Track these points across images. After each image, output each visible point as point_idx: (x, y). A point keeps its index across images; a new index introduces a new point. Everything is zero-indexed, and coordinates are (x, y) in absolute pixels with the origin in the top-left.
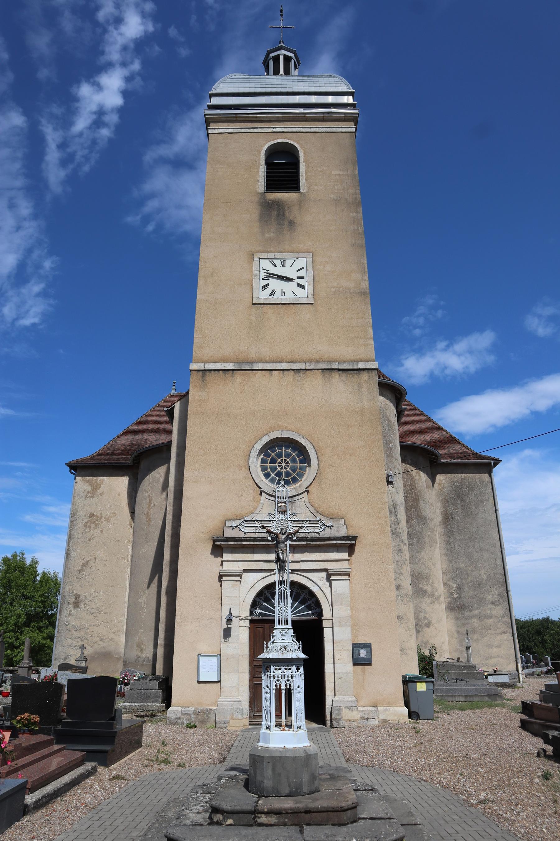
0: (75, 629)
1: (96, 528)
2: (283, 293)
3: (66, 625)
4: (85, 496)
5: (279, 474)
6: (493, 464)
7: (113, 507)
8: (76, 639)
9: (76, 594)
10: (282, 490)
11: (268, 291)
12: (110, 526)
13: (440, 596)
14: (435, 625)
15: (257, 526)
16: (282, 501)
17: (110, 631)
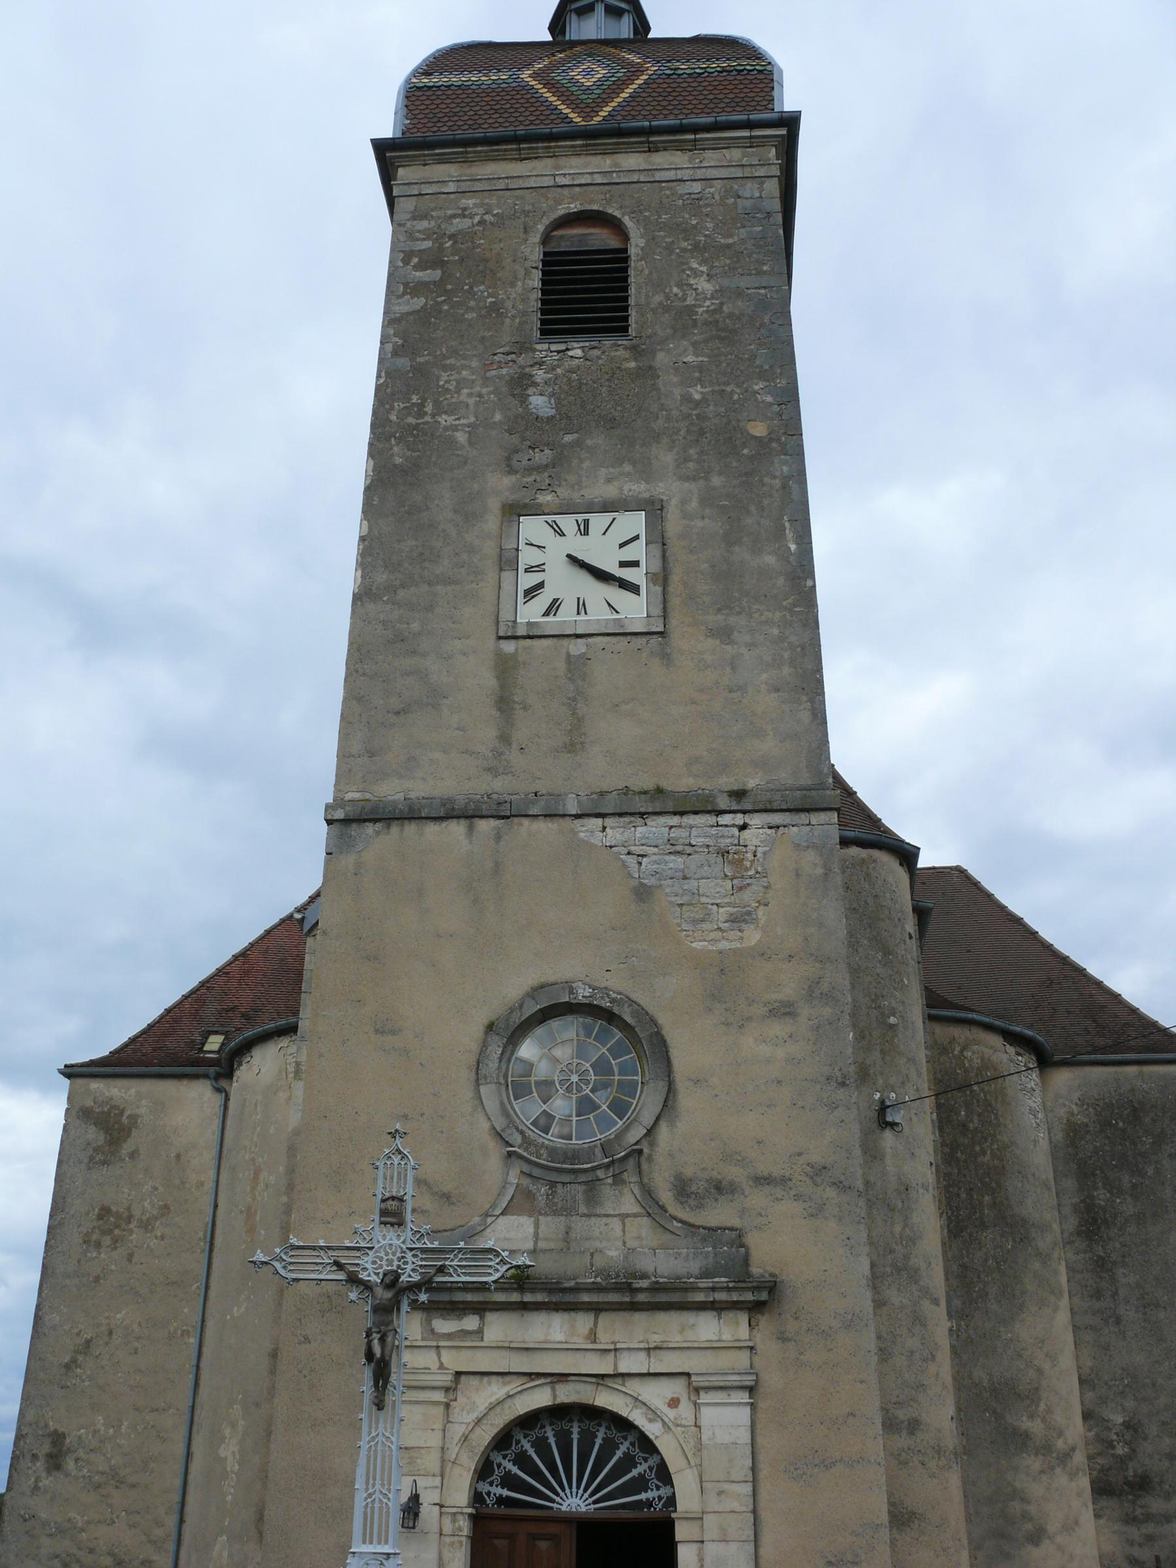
0: (48, 1532)
1: (116, 1248)
2: (581, 607)
3: (25, 1520)
4: (86, 1160)
7: (161, 1189)
9: (56, 1431)
10: (396, 1163)
12: (153, 1243)
13: (1073, 1449)
14: (1059, 1539)
15: (323, 1263)
16: (394, 1194)
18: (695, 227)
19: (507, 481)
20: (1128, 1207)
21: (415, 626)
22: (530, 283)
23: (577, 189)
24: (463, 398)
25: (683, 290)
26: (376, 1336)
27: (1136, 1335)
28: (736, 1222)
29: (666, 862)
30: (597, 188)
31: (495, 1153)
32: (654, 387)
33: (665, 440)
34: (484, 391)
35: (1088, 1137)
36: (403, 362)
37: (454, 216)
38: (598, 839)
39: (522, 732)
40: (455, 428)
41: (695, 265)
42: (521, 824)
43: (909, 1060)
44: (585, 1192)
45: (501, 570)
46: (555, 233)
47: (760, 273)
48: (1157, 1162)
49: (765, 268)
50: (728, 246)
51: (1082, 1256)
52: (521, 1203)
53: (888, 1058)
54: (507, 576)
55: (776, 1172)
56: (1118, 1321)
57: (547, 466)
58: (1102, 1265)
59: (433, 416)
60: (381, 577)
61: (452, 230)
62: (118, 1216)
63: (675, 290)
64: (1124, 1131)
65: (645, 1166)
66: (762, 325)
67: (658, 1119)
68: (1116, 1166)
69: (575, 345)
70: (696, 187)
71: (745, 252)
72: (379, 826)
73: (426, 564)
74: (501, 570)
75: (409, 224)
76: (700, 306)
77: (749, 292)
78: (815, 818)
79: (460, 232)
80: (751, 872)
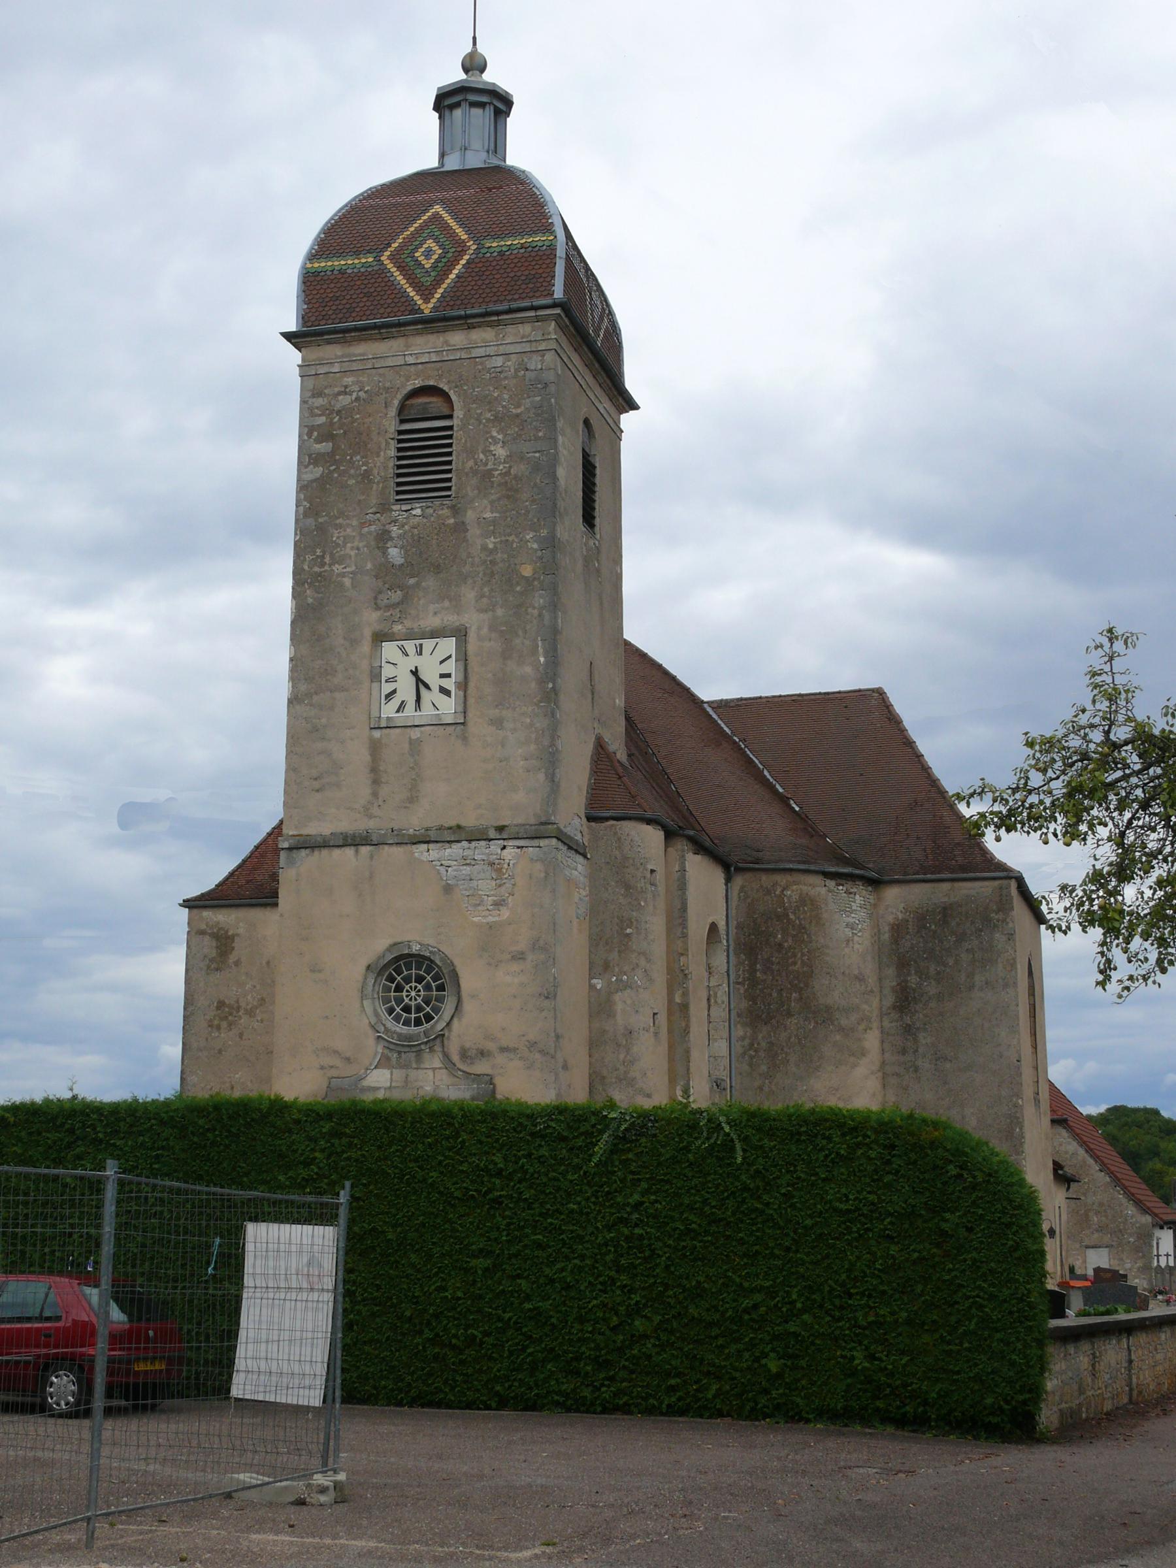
1: (231, 1029)
4: (205, 968)
5: (407, 1009)
7: (258, 987)
11: (395, 703)
12: (256, 1025)
18: (496, 399)
19: (375, 615)
20: (932, 989)
21: (324, 721)
22: (388, 452)
23: (420, 366)
24: (348, 551)
25: (485, 455)
27: (928, 1080)
28: (489, 1072)
29: (461, 871)
30: (433, 365)
31: (372, 1035)
32: (465, 540)
33: (470, 581)
34: (361, 545)
35: (908, 937)
36: (310, 522)
37: (339, 393)
38: (425, 857)
39: (384, 791)
40: (343, 575)
41: (495, 434)
42: (383, 849)
44: (416, 1056)
45: (372, 681)
46: (407, 402)
47: (537, 439)
49: (540, 434)
50: (517, 416)
51: (894, 1024)
52: (385, 1062)
54: (375, 685)
55: (511, 1045)
56: (916, 1069)
57: (398, 603)
58: (908, 1030)
59: (330, 565)
60: (303, 687)
61: (338, 407)
63: (482, 456)
64: (935, 932)
65: (446, 1042)
66: (535, 484)
67: (452, 1017)
68: (926, 958)
69: (418, 505)
70: (499, 362)
71: (529, 420)
72: (308, 851)
73: (329, 677)
74: (372, 681)
75: (311, 400)
76: (497, 470)
77: (529, 455)
78: (543, 843)
79: (344, 408)
80: (506, 876)
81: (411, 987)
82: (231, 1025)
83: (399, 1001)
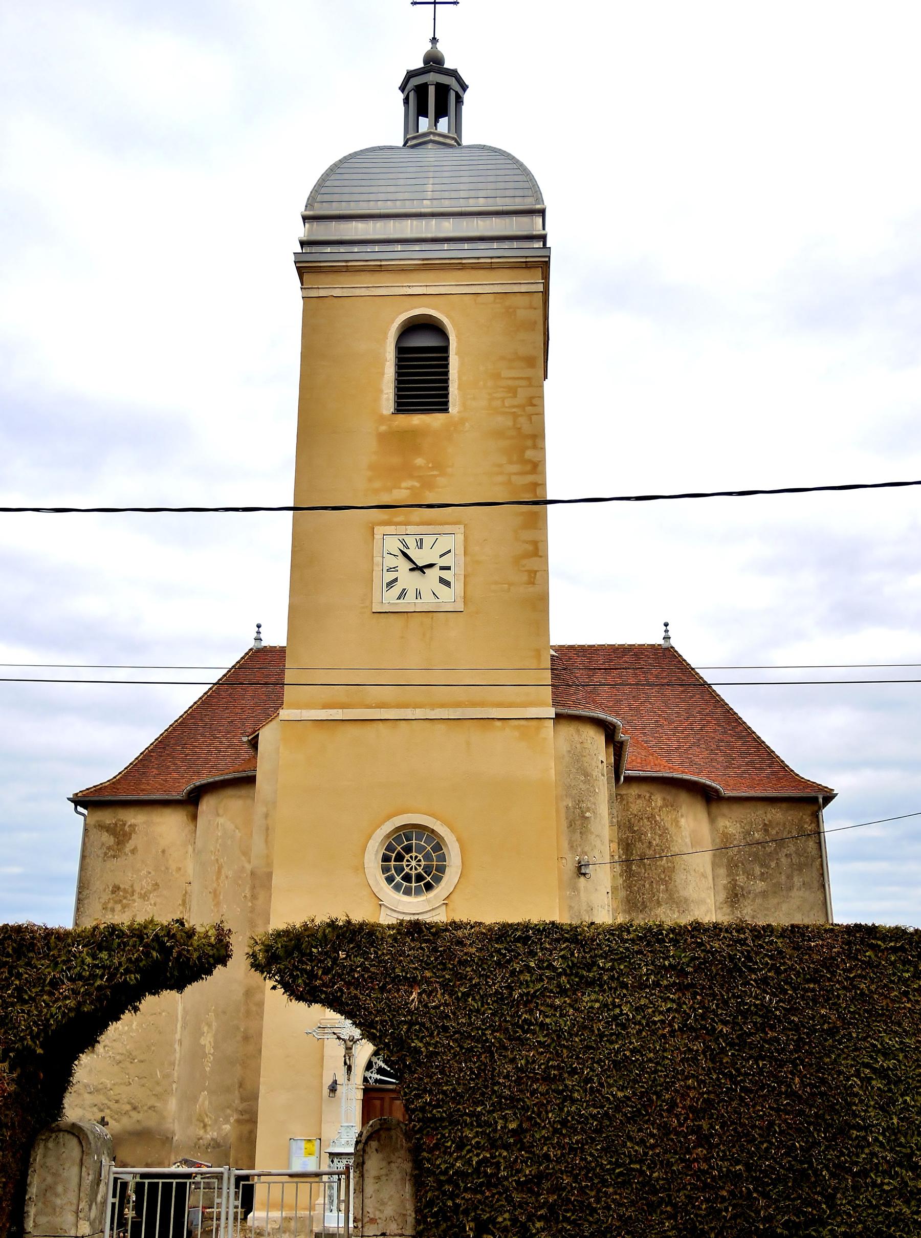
0: (89, 1091)
1: (124, 912)
2: (418, 594)
4: (102, 855)
5: (407, 878)
6: (821, 800)
7: (153, 873)
8: (90, 1107)
11: (396, 590)
17: (150, 1093)
20: (760, 885)
26: (347, 1057)
43: (597, 836)
48: (777, 859)
53: (584, 836)
62: (125, 890)
68: (752, 861)
81: (411, 857)
82: (125, 908)
83: (399, 870)
